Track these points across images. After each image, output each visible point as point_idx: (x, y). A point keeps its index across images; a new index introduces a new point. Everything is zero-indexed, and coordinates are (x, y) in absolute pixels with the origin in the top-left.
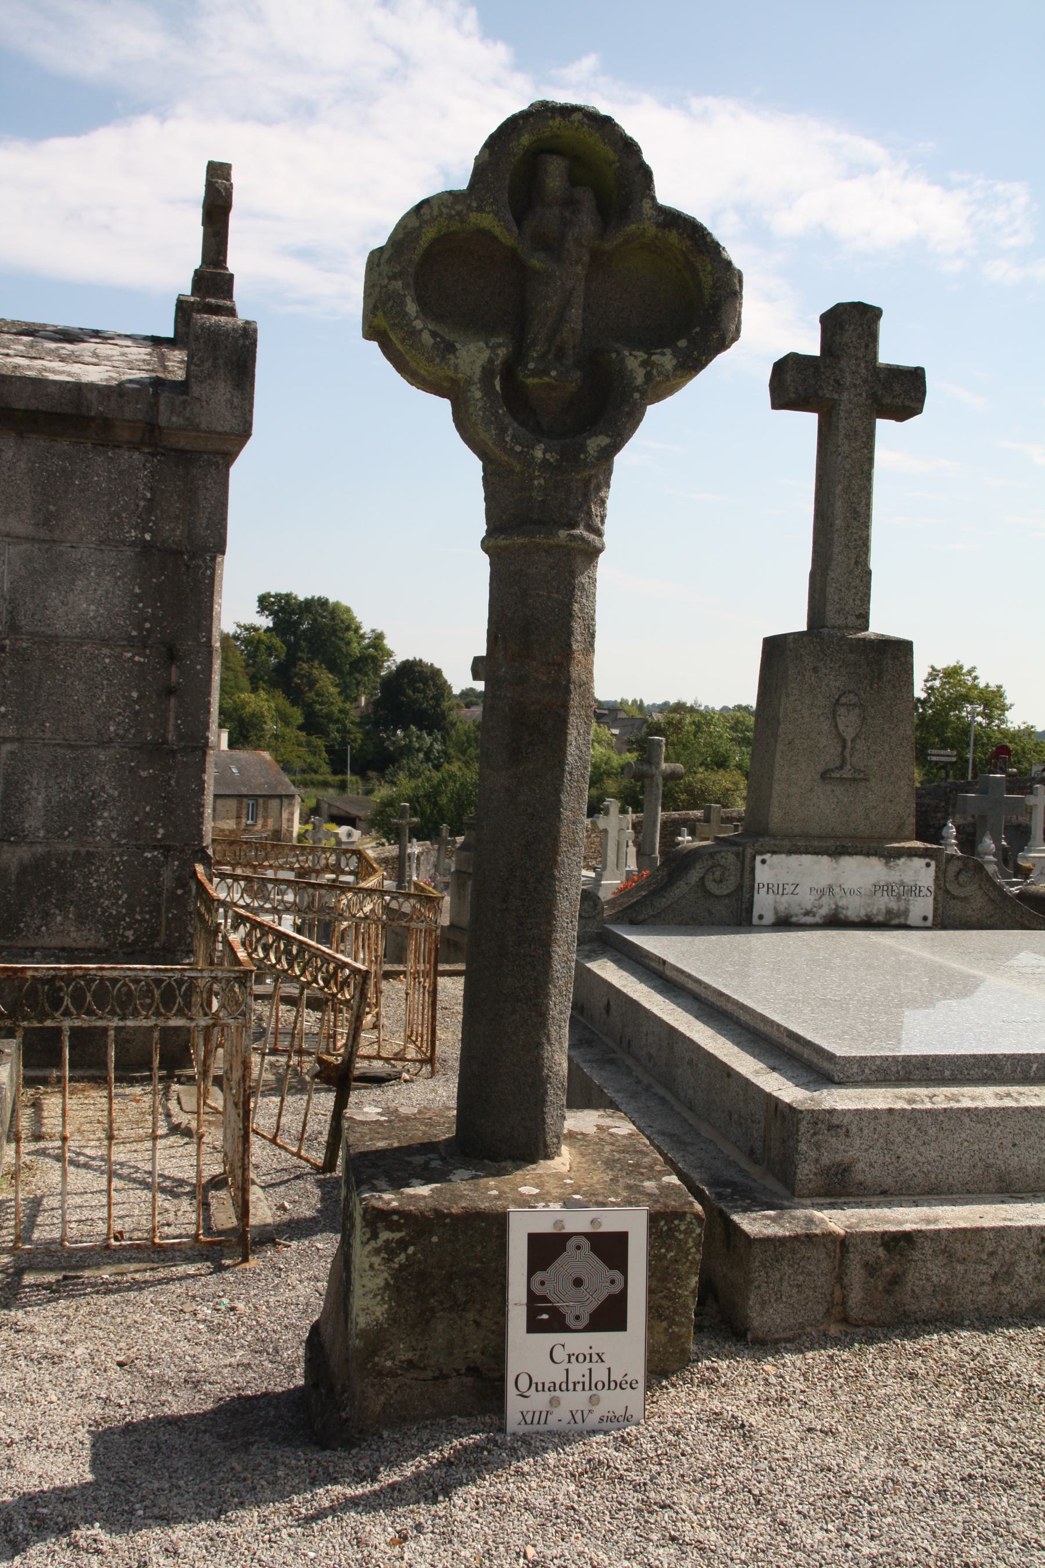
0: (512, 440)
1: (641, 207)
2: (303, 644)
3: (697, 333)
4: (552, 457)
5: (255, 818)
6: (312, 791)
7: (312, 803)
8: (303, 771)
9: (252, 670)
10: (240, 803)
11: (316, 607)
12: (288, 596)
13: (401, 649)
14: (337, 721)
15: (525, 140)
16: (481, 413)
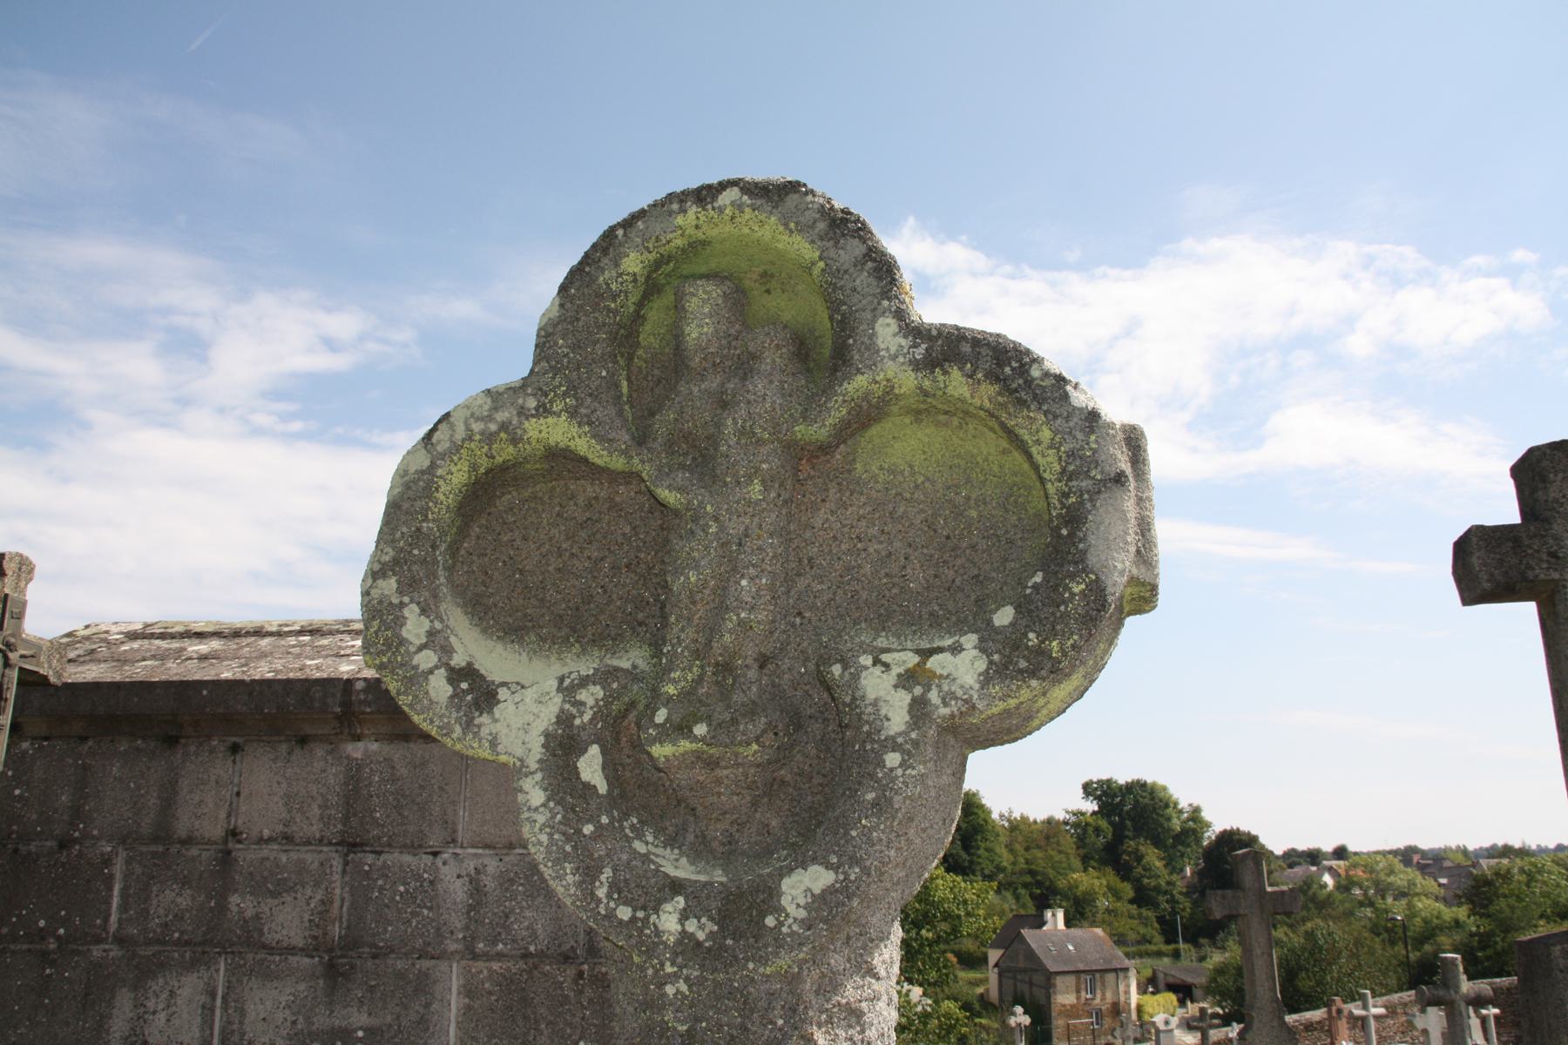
0: (609, 896)
1: (873, 336)
2: (1128, 823)
3: (1036, 587)
4: (701, 927)
5: (1093, 991)
6: (1148, 961)
7: (1148, 973)
8: (1139, 943)
9: (1082, 852)
10: (1078, 980)
11: (1137, 788)
12: (1109, 781)
13: (1219, 820)
14: (1166, 893)
15: (633, 263)
16: (544, 838)
